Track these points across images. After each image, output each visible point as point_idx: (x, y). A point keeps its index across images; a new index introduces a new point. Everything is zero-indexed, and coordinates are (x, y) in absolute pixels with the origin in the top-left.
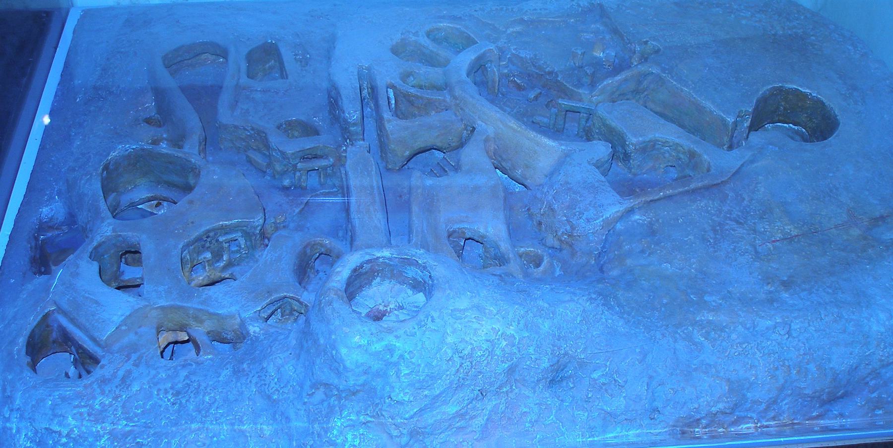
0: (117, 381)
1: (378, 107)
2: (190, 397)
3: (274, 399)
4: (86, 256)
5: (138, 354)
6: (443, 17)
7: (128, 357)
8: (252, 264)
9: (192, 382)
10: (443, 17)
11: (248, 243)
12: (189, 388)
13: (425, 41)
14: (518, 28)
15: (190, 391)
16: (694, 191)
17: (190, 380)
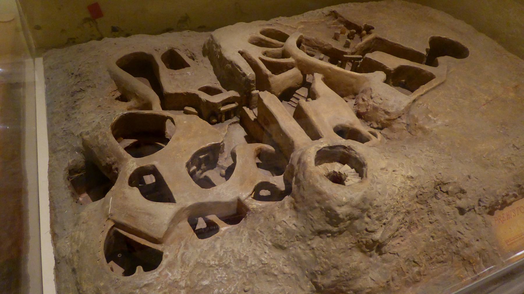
0: (179, 263)
2: (231, 260)
3: (79, 199)
5: (184, 240)
9: (226, 249)
12: (227, 254)
14: (302, 26)
15: (228, 256)
17: (224, 248)
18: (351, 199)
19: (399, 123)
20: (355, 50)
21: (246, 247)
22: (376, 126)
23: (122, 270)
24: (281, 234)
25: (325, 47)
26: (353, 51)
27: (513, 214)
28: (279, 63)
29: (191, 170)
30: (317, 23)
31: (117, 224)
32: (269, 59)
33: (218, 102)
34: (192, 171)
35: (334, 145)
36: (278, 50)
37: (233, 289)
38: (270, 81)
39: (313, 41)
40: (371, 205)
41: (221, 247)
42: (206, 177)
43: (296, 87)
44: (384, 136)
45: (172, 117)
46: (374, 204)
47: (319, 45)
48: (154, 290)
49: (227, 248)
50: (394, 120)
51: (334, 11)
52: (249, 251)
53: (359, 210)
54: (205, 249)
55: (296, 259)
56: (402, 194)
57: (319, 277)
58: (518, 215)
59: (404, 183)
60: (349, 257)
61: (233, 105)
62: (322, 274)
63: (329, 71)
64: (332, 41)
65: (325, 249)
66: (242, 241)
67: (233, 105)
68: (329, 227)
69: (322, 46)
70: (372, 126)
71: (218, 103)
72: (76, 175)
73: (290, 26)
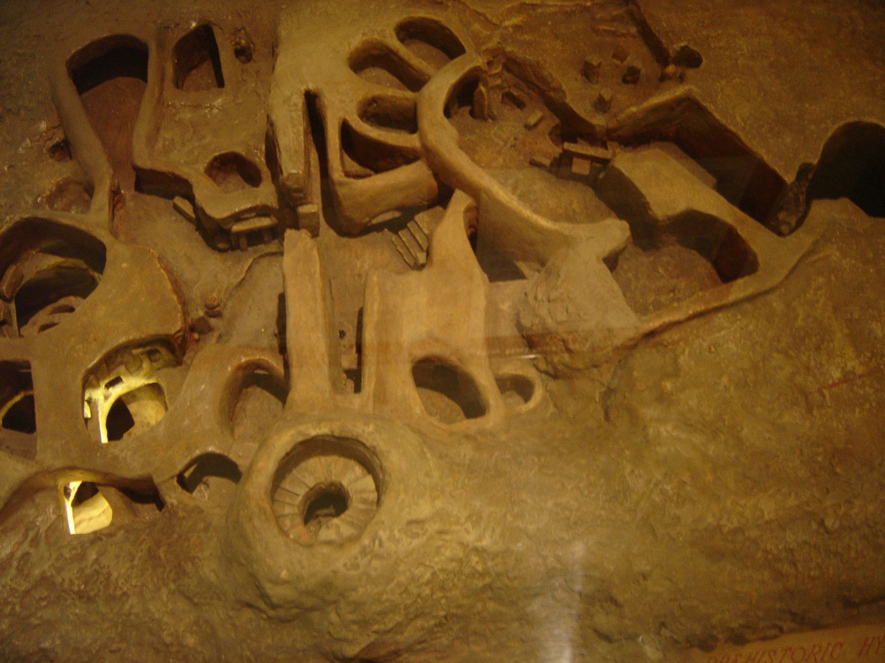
7: (26, 536)
14: (516, 20)
18: (298, 577)
20: (616, 123)
21: (134, 575)
22: (543, 366)
25: (552, 94)
26: (611, 125)
30: (568, 9)
35: (343, 435)
36: (407, 99)
39: (529, 69)
40: (341, 595)
41: (96, 561)
44: (551, 393)
45: (106, 246)
47: (540, 85)
49: (102, 565)
50: (578, 370)
52: (136, 586)
55: (208, 630)
64: (576, 80)
66: (132, 560)
69: (546, 88)
70: (535, 362)
73: (484, 15)
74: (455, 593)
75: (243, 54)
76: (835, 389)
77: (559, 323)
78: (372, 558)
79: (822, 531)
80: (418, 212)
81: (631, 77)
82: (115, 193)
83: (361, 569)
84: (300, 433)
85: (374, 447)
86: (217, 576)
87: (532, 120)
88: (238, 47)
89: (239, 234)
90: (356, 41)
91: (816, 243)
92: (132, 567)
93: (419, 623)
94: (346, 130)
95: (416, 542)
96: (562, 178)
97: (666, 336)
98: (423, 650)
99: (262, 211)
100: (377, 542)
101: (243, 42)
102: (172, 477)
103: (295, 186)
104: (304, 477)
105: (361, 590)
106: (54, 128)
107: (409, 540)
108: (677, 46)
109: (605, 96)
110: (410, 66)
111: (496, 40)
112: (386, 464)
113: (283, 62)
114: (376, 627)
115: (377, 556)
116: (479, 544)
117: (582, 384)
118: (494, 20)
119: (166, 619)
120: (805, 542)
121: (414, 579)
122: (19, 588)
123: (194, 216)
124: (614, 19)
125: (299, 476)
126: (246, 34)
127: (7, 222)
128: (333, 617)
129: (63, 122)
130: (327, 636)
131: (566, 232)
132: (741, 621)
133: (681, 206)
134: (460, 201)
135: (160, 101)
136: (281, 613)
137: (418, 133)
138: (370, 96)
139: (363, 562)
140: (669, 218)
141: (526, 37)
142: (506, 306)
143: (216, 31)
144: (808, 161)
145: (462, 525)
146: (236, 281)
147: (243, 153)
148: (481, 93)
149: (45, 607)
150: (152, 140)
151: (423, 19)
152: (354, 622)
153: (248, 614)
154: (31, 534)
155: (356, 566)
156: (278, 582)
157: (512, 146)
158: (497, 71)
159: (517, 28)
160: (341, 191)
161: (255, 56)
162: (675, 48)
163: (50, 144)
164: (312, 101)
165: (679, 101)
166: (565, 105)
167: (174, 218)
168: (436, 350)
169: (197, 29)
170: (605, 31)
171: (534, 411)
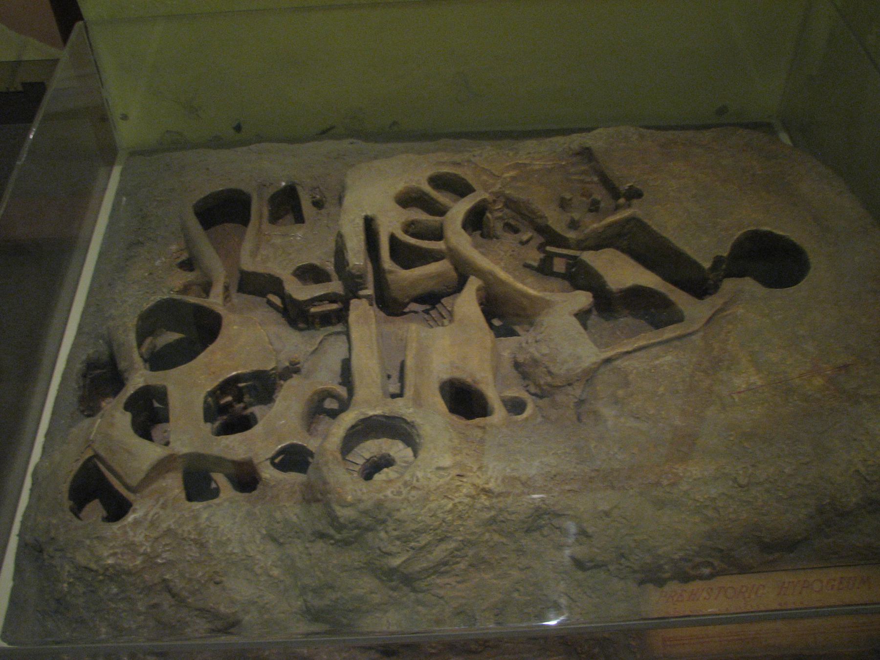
1: (123, 484)
4: (121, 406)
6: (444, 163)
7: (157, 501)
8: (65, 585)
10: (444, 163)
11: (508, 180)
13: (427, 188)
14: (512, 173)
16: (667, 341)
19: (568, 395)
22: (533, 389)
23: (105, 513)
24: (278, 523)
26: (580, 238)
27: (705, 594)
28: (420, 249)
29: (223, 401)
31: (96, 456)
32: (405, 239)
33: (303, 299)
34: (224, 404)
35: (393, 414)
36: (436, 221)
37: (200, 574)
38: (389, 279)
40: (389, 514)
41: (208, 519)
42: (252, 413)
43: (445, 291)
46: (394, 516)
48: (105, 545)
50: (558, 387)
51: (587, 148)
52: (237, 534)
53: (371, 519)
54: (187, 516)
56: (460, 513)
57: (310, 594)
58: (716, 599)
59: (473, 497)
60: (354, 580)
61: (334, 306)
62: (314, 591)
63: (490, 277)
65: (323, 559)
67: (334, 306)
68: (332, 532)
70: (528, 388)
71: (303, 301)
72: (98, 371)
74: (470, 523)
75: (318, 204)
76: (742, 395)
77: (544, 355)
78: (412, 488)
79: (736, 485)
80: (443, 297)
81: (594, 207)
82: (226, 288)
83: (403, 496)
84: (363, 413)
85: (413, 422)
86: (298, 517)
87: (525, 238)
88: (314, 199)
89: (314, 315)
90: (400, 186)
91: (726, 303)
92: (234, 523)
93: (443, 546)
94: (393, 239)
95: (442, 481)
96: (547, 275)
97: (617, 363)
98: (446, 572)
99: (330, 298)
100: (415, 479)
101: (318, 197)
102: (267, 459)
103: (358, 273)
104: (362, 452)
105: (403, 511)
106: (182, 250)
107: (437, 479)
108: (627, 186)
109: (575, 217)
110: (437, 202)
111: (498, 186)
112: (421, 432)
113: (348, 200)
114: (413, 544)
115: (414, 488)
116: (487, 486)
117: (560, 398)
118: (497, 174)
119: (258, 557)
120: (724, 494)
121: (440, 507)
122: (152, 535)
123: (281, 306)
124: (583, 173)
125: (359, 452)
126: (320, 191)
127: (152, 301)
128: (382, 534)
129: (189, 243)
130: (378, 551)
131: (548, 298)
132: (681, 554)
133: (629, 283)
134: (473, 284)
135: (259, 230)
136: (345, 534)
137: (444, 239)
138: (410, 219)
139: (404, 491)
140: (621, 291)
141: (520, 184)
142: (506, 354)
143: (299, 188)
144: (720, 254)
145: (474, 473)
146: (311, 350)
147: (318, 264)
148: (487, 218)
149: (168, 551)
150: (254, 254)
151: (448, 173)
152: (398, 538)
153: (320, 544)
154: (162, 501)
155: (399, 493)
156: (345, 505)
157: (511, 256)
158: (500, 207)
159: (513, 178)
160: (390, 277)
161: (327, 205)
162: (624, 187)
163: (179, 261)
164: (370, 227)
165: (628, 220)
166: (548, 227)
167: (266, 310)
168: (458, 375)
169: (285, 187)
170: (575, 180)
171: (527, 419)
